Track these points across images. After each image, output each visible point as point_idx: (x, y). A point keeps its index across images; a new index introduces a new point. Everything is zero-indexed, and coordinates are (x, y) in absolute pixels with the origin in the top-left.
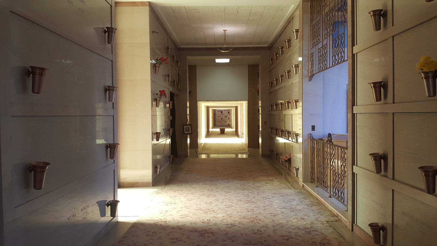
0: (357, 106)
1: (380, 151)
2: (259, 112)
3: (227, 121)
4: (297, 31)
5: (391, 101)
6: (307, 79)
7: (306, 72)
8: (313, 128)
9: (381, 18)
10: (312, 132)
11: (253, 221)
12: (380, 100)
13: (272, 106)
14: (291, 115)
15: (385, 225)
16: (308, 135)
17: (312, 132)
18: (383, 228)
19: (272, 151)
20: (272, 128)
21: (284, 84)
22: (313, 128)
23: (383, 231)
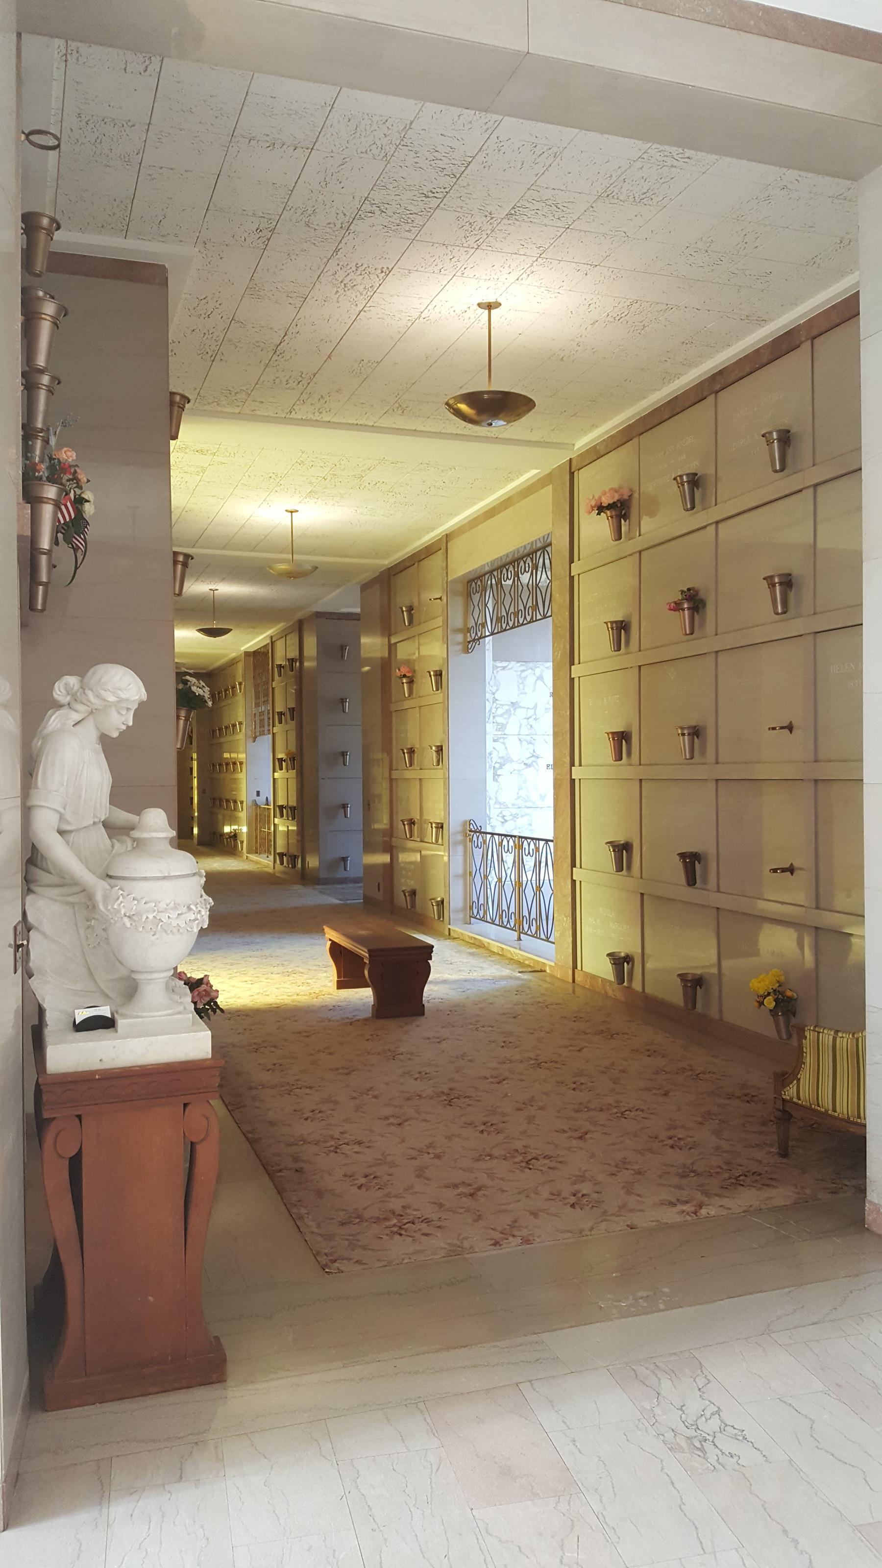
0: (580, 765)
1: (621, 839)
2: (192, 773)
3: (763, 906)
4: (240, 684)
5: (713, 760)
6: (251, 740)
7: (250, 733)
8: (258, 794)
9: (622, 631)
10: (257, 798)
11: (337, 1148)
12: (621, 759)
13: (213, 765)
14: (418, 782)
15: (629, 954)
16: (465, 823)
17: (257, 798)
18: (628, 959)
19: (214, 833)
20: (214, 799)
21: (228, 738)
22: (258, 794)
23: (628, 964)
